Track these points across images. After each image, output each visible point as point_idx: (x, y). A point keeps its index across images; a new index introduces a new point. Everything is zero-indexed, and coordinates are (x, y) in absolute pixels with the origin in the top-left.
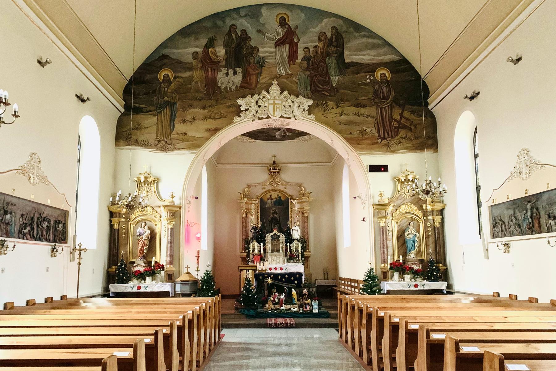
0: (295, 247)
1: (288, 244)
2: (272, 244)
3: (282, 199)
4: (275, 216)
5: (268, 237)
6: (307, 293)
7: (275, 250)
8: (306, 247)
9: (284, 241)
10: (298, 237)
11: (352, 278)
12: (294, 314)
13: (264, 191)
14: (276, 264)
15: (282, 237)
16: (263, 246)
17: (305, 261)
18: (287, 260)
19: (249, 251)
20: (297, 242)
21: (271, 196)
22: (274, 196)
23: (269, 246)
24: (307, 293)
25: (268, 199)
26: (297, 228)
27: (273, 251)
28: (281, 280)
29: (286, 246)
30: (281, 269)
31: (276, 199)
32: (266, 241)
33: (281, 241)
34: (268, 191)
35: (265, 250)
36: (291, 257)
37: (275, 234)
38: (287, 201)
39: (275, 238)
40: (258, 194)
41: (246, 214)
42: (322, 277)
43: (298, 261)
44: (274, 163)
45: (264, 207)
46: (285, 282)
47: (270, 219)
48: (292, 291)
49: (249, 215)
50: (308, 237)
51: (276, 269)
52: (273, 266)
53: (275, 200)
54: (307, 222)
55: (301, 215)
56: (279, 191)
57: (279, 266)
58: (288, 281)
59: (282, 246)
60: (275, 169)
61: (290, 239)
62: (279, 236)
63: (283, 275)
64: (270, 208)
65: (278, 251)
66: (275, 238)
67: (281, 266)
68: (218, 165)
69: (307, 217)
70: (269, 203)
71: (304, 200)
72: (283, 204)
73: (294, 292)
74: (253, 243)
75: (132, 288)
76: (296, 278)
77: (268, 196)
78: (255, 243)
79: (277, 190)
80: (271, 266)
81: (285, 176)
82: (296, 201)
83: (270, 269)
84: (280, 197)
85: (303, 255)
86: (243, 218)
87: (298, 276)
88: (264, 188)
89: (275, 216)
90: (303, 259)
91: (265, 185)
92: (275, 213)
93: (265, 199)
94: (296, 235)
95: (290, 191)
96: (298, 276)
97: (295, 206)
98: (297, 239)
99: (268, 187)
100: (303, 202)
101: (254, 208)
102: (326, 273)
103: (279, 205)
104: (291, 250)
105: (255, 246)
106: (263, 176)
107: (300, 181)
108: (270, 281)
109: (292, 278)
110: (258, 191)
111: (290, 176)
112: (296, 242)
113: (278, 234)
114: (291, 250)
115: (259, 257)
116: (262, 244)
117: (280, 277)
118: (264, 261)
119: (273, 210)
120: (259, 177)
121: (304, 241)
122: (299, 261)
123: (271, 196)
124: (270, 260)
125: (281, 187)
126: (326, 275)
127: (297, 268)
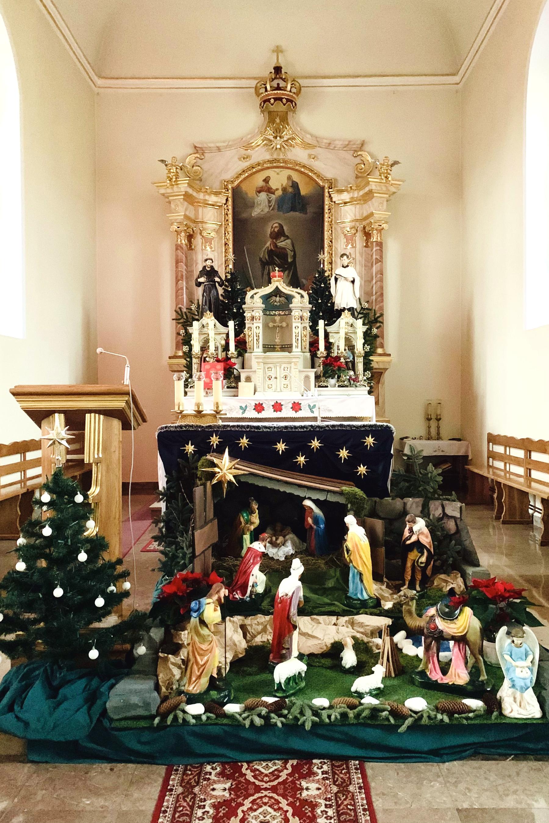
0: (342, 335)
1: (321, 323)
2: (266, 326)
3: (304, 191)
4: (275, 246)
5: (254, 302)
6: (426, 540)
7: (277, 345)
8: (376, 336)
9: (307, 315)
10: (355, 305)
11: (536, 438)
12: (371, 735)
13: (245, 164)
14: (280, 389)
15: (301, 303)
16: (237, 334)
17: (375, 378)
18: (317, 377)
19: (191, 347)
20: (351, 320)
21: (266, 180)
22: (279, 180)
23: (255, 330)
24: (426, 540)
25: (260, 191)
26: (351, 273)
27: (269, 348)
28: (285, 463)
29: (315, 331)
30: (296, 407)
31: (284, 190)
32: (247, 315)
33: (296, 313)
34: (260, 167)
35: (242, 346)
36: (330, 369)
37: (277, 292)
38: (319, 196)
39: (277, 304)
40: (229, 176)
41: (190, 237)
42: (422, 431)
43: (353, 382)
44: (278, 70)
45: (244, 215)
46: (307, 470)
47: (263, 254)
48: (345, 529)
49: (198, 241)
50: (382, 308)
51: (277, 407)
52: (267, 397)
53: (279, 193)
54: (380, 260)
55: (359, 239)
56: (295, 166)
57: (287, 397)
58: (323, 465)
59: (299, 328)
60: (278, 88)
61: (325, 310)
62: (289, 298)
63: (297, 438)
64: (263, 220)
65: (287, 348)
66: (277, 304)
67: (297, 397)
68: (100, 82)
69: (380, 244)
70: (261, 205)
71: (373, 186)
72: (306, 207)
73: (356, 537)
74: (204, 320)
75: (244, 409)
76: (359, 454)
77: (259, 180)
78: (209, 319)
79: (285, 165)
80: (260, 397)
81: (311, 119)
82: (346, 197)
83: (259, 408)
84: (295, 185)
85: (367, 366)
86: (178, 247)
87: (370, 441)
88: (246, 158)
89: (275, 246)
90: (368, 374)
91: (248, 146)
92: (279, 234)
93: (249, 189)
94: (344, 295)
95: (327, 167)
96: (370, 441)
97: (343, 216)
98: (351, 310)
99: (260, 154)
100: (370, 195)
101: (214, 221)
102: (433, 418)
103: (293, 209)
104: (329, 346)
105: (209, 331)
106: (245, 120)
107: (355, 134)
108: (226, 467)
109: (344, 453)
110: (228, 167)
111: (325, 125)
112: (346, 317)
113: (287, 290)
114: (329, 346)
115: (220, 366)
116: (231, 324)
117: (281, 447)
118: (238, 379)
119: (272, 226)
120: (232, 127)
121: (371, 317)
122: (356, 380)
123: (266, 180)
124: (258, 377)
125: (299, 154)
126: (433, 424)
127: (349, 404)
